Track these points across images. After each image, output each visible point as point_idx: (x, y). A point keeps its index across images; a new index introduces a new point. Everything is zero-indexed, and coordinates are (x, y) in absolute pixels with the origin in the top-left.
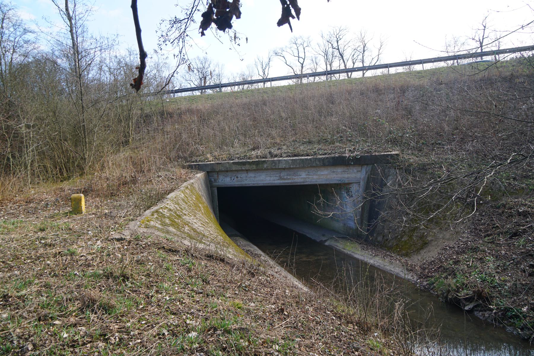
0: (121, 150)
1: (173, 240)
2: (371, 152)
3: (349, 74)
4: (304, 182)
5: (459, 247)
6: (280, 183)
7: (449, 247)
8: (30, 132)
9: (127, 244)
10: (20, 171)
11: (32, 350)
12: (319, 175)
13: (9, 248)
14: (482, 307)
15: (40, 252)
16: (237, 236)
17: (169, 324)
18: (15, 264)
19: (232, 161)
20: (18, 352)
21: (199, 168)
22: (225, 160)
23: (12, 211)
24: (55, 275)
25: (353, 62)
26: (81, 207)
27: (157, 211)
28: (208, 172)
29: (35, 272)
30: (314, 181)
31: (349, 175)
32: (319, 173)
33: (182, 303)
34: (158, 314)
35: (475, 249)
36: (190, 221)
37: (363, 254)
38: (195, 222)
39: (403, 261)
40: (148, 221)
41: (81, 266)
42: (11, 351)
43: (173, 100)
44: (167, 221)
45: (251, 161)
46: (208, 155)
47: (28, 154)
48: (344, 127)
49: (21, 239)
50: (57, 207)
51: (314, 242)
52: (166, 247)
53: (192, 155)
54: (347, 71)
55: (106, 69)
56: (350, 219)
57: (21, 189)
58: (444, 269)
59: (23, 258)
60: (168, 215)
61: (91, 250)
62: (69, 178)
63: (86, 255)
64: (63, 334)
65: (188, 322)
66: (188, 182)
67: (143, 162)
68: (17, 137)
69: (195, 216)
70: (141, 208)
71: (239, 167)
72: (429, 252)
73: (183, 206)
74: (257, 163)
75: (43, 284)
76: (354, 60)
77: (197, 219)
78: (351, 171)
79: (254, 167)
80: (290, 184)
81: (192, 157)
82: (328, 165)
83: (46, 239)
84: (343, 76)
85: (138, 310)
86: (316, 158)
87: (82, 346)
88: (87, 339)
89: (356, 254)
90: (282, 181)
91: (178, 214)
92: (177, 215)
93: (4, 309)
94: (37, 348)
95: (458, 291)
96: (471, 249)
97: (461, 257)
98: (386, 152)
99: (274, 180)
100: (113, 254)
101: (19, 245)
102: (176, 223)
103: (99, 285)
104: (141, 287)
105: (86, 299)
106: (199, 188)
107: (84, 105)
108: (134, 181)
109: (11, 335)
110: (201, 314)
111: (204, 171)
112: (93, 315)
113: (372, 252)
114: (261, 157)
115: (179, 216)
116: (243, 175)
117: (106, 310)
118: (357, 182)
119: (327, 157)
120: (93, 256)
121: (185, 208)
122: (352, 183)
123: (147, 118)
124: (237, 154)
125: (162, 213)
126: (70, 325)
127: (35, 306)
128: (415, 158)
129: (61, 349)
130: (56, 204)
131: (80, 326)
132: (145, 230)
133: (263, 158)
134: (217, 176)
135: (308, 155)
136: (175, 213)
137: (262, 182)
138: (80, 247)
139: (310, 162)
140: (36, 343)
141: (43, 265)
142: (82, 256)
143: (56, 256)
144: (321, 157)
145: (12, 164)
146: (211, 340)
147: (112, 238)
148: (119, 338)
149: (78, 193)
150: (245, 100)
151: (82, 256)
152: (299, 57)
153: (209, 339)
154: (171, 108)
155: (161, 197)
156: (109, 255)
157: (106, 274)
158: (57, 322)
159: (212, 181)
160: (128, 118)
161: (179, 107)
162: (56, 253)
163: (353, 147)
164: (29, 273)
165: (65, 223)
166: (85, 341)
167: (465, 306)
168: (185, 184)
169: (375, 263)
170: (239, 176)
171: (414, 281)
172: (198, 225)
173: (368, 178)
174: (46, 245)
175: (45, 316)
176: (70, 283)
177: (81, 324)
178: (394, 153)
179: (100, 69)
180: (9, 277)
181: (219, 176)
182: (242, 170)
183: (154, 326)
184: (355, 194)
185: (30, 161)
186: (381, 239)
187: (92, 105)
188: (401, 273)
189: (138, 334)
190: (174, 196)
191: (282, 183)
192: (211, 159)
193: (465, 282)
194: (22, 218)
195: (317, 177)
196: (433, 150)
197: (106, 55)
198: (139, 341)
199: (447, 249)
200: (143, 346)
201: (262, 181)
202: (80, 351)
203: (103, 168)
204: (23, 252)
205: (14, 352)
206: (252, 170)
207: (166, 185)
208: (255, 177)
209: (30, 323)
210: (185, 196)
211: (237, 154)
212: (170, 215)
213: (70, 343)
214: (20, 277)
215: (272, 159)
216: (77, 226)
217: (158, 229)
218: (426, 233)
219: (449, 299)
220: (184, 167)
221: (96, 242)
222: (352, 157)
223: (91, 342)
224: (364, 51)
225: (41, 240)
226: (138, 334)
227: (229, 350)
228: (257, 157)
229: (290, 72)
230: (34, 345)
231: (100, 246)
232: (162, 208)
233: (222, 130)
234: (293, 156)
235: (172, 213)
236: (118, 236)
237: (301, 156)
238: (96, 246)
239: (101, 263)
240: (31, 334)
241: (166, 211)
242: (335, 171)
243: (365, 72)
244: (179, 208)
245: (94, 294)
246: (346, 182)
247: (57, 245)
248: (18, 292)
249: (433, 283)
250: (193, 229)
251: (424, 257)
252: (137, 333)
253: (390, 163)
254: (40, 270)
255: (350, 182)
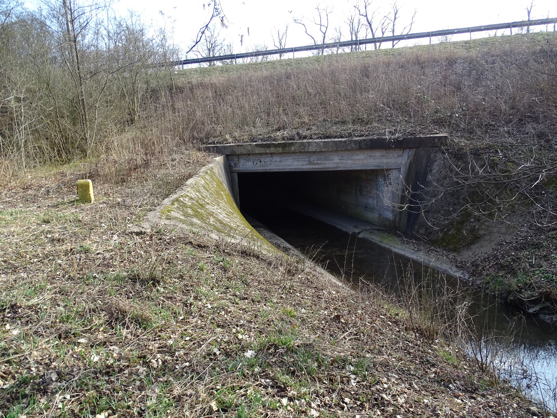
0: (127, 128)
1: (200, 233)
2: (415, 134)
3: (378, 44)
4: (336, 168)
5: (517, 242)
6: (309, 169)
7: (506, 242)
8: (21, 106)
9: (148, 239)
10: (12, 153)
11: (56, 381)
12: (353, 160)
13: (9, 243)
14: (551, 310)
15: (47, 249)
16: (260, 227)
17: (219, 340)
18: (20, 264)
19: (254, 143)
20: (39, 383)
21: (218, 151)
22: (247, 142)
23: (7, 199)
24: (70, 278)
25: (382, 32)
26: (90, 194)
27: (177, 200)
28: (227, 155)
29: (45, 274)
30: (348, 166)
31: (388, 160)
32: (354, 157)
33: (227, 312)
34: (202, 328)
35: (537, 245)
36: (214, 211)
37: (403, 248)
38: (220, 213)
39: (451, 256)
40: (169, 211)
41: (99, 266)
42: (30, 382)
43: (182, 73)
44: (190, 211)
45: (277, 143)
46: (227, 136)
47: (20, 132)
48: (382, 105)
49: (22, 233)
50: (60, 194)
51: (346, 234)
52: (193, 242)
53: (208, 136)
54: (373, 41)
55: (105, 32)
56: (387, 210)
57: (15, 174)
58: (501, 267)
59: (28, 256)
60: (190, 204)
61: (108, 246)
62: (69, 161)
63: (103, 252)
64: (94, 358)
65: (240, 337)
66: (206, 166)
67: (153, 143)
68: (7, 112)
69: (218, 205)
70: (158, 196)
71: (262, 150)
72: (482, 247)
73: (204, 193)
74: (283, 146)
75: (58, 290)
76: (384, 30)
77: (221, 208)
78: (391, 155)
79: (280, 150)
80: (320, 170)
81: (208, 138)
82: (365, 149)
83: (53, 233)
84: (370, 47)
85: (177, 322)
86: (351, 141)
87: (119, 373)
88: (124, 363)
89: (396, 248)
90: (311, 167)
91: (201, 203)
92: (200, 204)
93: (13, 322)
94: (63, 378)
95: (520, 292)
96: (533, 245)
97: (521, 255)
98: (433, 134)
99: (303, 165)
100: (134, 251)
101: (22, 241)
102: (199, 213)
103: (125, 291)
104: (175, 293)
105: (113, 309)
106: (219, 174)
107: (82, 75)
108: (146, 164)
109: (27, 359)
110: (253, 326)
111: (222, 154)
112: (125, 330)
113: (414, 246)
114: (287, 138)
115: (202, 206)
116: (268, 159)
117: (139, 324)
118: (397, 167)
119: (365, 140)
120: (111, 253)
121: (207, 196)
122: (391, 169)
123: (154, 93)
124: (261, 135)
125: (183, 202)
126: (99, 345)
127: (52, 319)
128: (466, 141)
129: (94, 378)
130: (58, 190)
131: (111, 346)
132: (167, 222)
133: (291, 139)
134: (237, 159)
135: (342, 137)
136: (198, 202)
137: (289, 167)
138: (94, 243)
139: (344, 144)
140: (61, 371)
141: (53, 266)
142: (98, 254)
143: (68, 254)
144: (356, 139)
145: (3, 145)
146: (274, 361)
147: (130, 231)
148: (162, 361)
149: (83, 179)
150: (265, 73)
151: (98, 254)
152: (321, 25)
153: (271, 360)
154: (181, 81)
155: (180, 183)
156: (130, 252)
157: (131, 277)
158: (82, 340)
159: (232, 165)
160: (134, 92)
161: (190, 80)
162: (67, 250)
163: (394, 128)
164: (38, 276)
165: (73, 213)
166: (121, 366)
167: (529, 308)
168: (204, 169)
169: (418, 258)
170: (263, 160)
171: (466, 279)
172: (222, 216)
173: (410, 163)
174: (52, 240)
175: (67, 332)
176: (90, 289)
177: (111, 343)
178: (442, 135)
179: (97, 33)
180: (15, 281)
181: (240, 160)
182: (267, 153)
183: (202, 343)
184: (394, 181)
185: (23, 141)
186: (424, 232)
187: (91, 75)
188: (449, 270)
189: (185, 354)
190: (194, 183)
191: (312, 169)
192: (230, 140)
193: (528, 282)
194: (21, 207)
195: (352, 162)
196: (486, 132)
197: (102, 15)
198: (187, 364)
199: (503, 244)
200: (193, 371)
201: (289, 166)
202: (118, 380)
203: (108, 149)
204: (27, 248)
205: (34, 383)
206: (277, 154)
207: (184, 171)
208: (281, 161)
209: (48, 342)
210: (206, 182)
211: (261, 135)
212: (192, 204)
213: (103, 369)
214: (28, 280)
215: (301, 141)
216: (87, 218)
217: (181, 221)
218: (477, 226)
219: (509, 300)
220: (199, 150)
221: (112, 237)
222: (393, 140)
223: (128, 366)
224: (395, 19)
225: (47, 233)
226: (185, 354)
227: (298, 374)
228: (283, 139)
229: (311, 43)
230: (59, 374)
231: (117, 242)
232: (182, 196)
233: (241, 108)
234: (325, 138)
235: (194, 202)
236: (136, 230)
237: (334, 138)
238: (112, 242)
239: (122, 262)
240: (52, 357)
241: (187, 199)
242: (372, 155)
243: (395, 42)
244: (200, 197)
245: (124, 303)
246: (385, 168)
247: (66, 240)
248: (28, 300)
249: (489, 282)
250: (219, 220)
251: (476, 253)
252: (183, 354)
253: (437, 147)
254: (51, 271)
255: (390, 168)
